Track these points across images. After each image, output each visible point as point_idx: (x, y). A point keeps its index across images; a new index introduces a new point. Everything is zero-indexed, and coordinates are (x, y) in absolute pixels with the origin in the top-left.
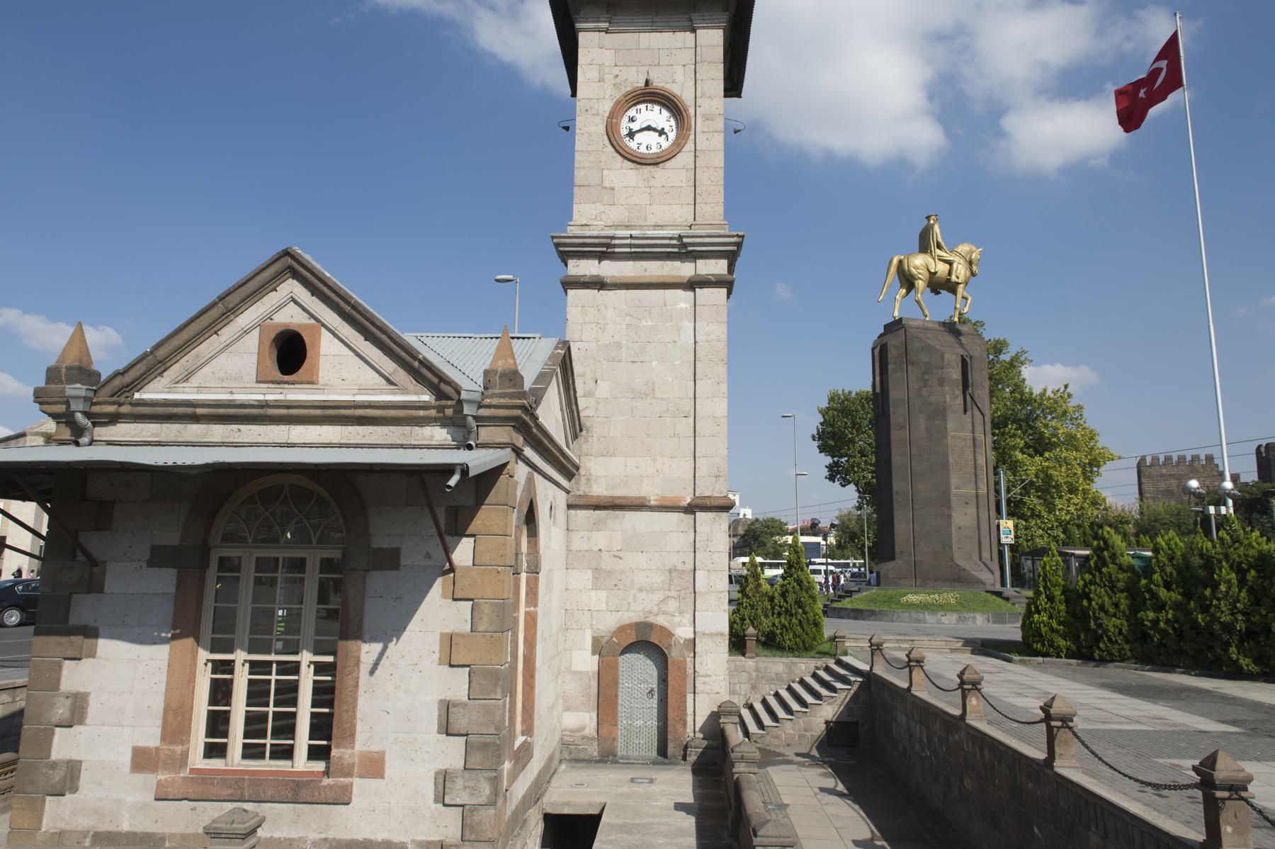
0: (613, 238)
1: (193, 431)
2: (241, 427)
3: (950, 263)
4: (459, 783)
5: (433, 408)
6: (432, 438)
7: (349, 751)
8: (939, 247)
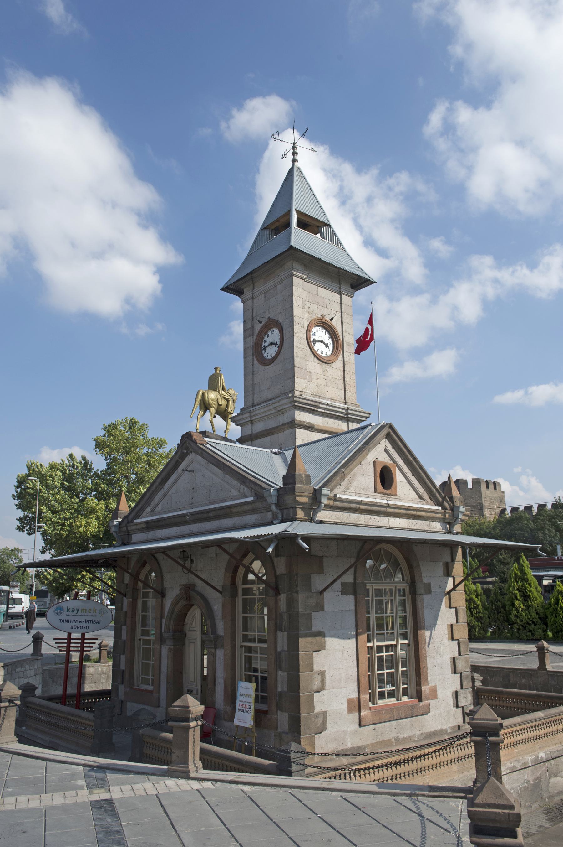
0: (320, 403)
1: (354, 517)
2: (371, 517)
3: (228, 400)
5: (441, 513)
6: (436, 528)
7: (427, 687)
8: (223, 389)
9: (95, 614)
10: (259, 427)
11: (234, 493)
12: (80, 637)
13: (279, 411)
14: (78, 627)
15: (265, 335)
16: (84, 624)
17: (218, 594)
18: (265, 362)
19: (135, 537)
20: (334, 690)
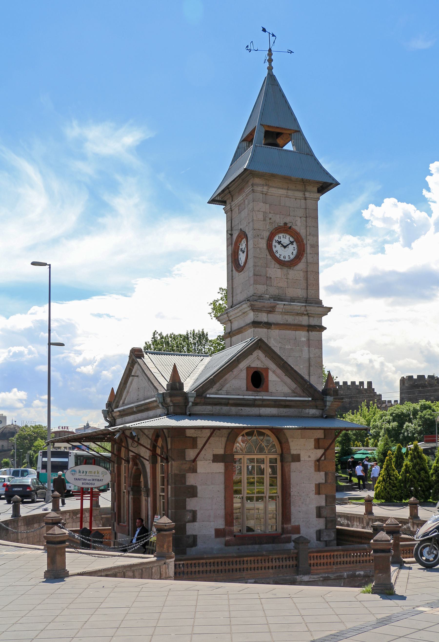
2: (242, 408)
4: (325, 534)
7: (290, 525)
9: (98, 475)
13: (244, 313)
15: (240, 244)
16: (91, 482)
19: (118, 421)
20: (203, 523)
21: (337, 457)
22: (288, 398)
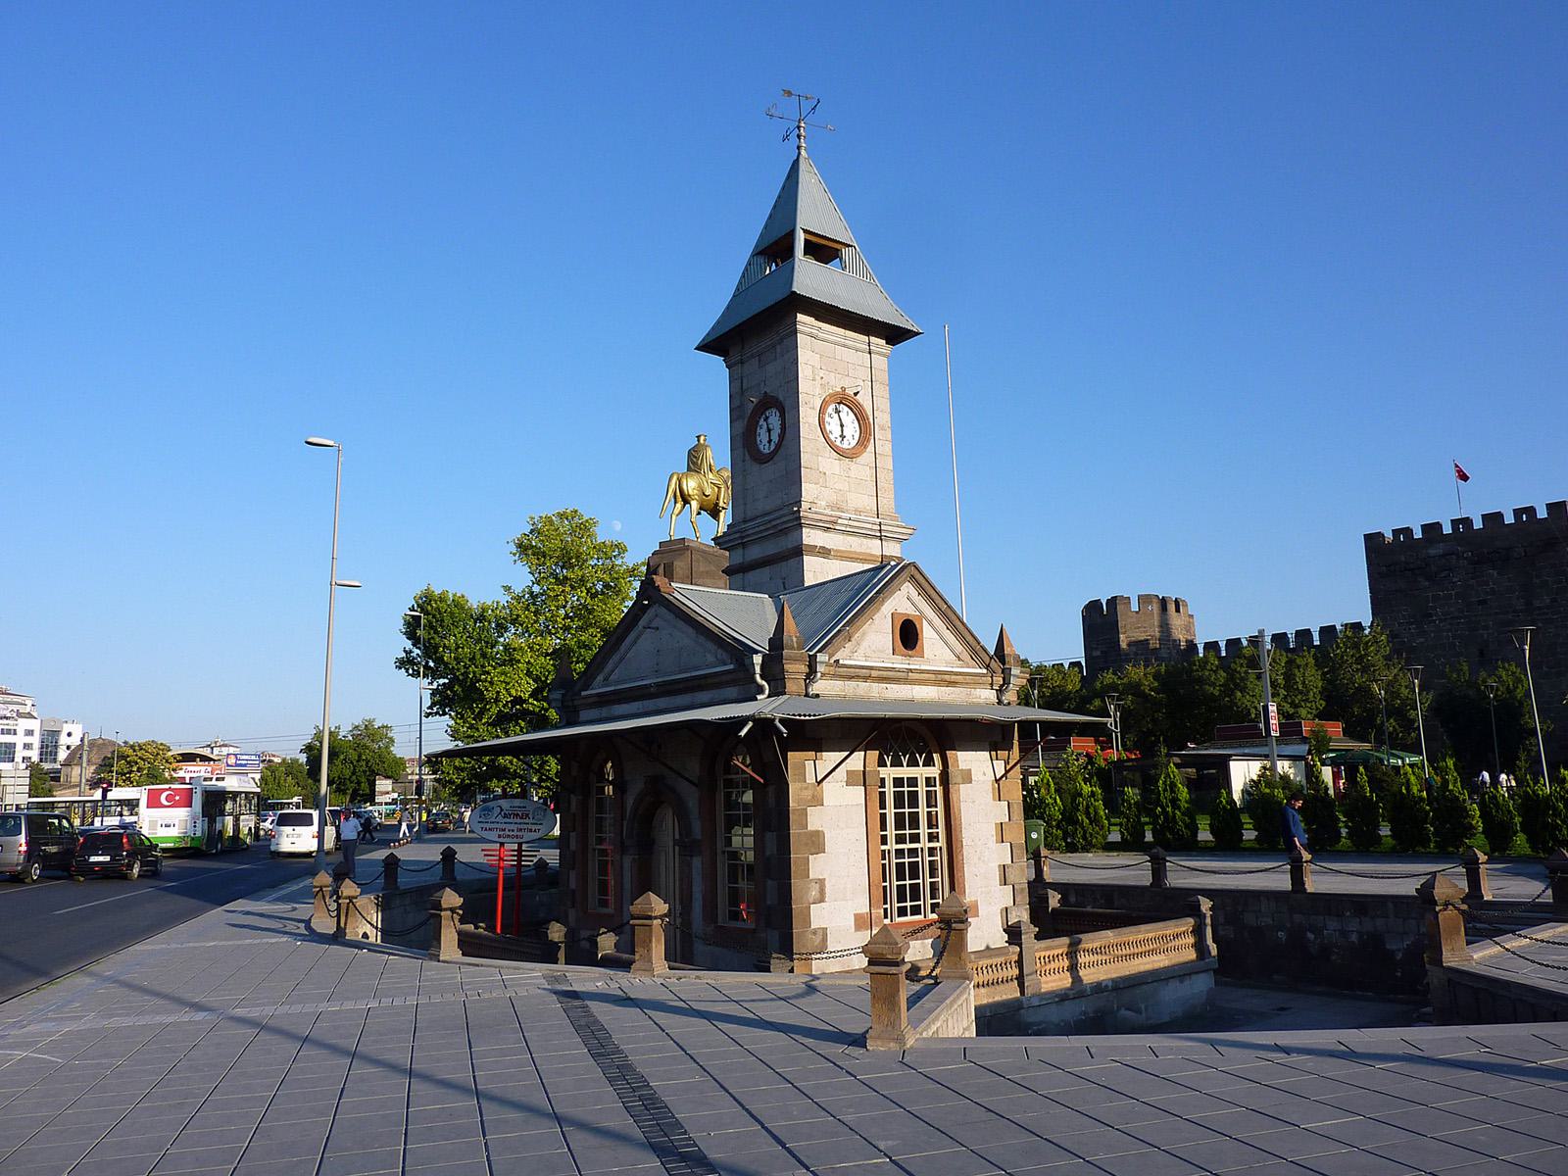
2: (888, 685)
10: (755, 552)
11: (710, 658)
12: (516, 848)
14: (513, 837)
17: (694, 788)
18: (761, 459)
19: (584, 715)
21: (1311, 774)
22: (697, 673)
